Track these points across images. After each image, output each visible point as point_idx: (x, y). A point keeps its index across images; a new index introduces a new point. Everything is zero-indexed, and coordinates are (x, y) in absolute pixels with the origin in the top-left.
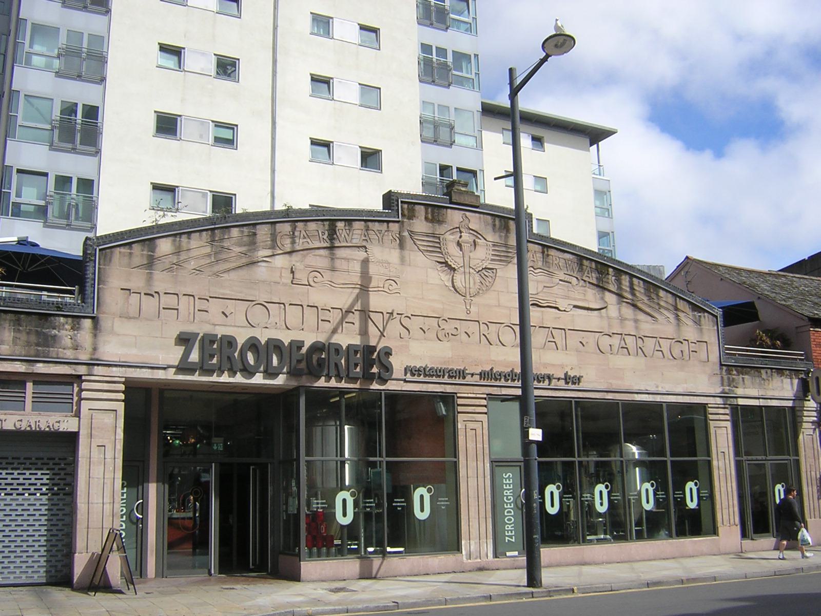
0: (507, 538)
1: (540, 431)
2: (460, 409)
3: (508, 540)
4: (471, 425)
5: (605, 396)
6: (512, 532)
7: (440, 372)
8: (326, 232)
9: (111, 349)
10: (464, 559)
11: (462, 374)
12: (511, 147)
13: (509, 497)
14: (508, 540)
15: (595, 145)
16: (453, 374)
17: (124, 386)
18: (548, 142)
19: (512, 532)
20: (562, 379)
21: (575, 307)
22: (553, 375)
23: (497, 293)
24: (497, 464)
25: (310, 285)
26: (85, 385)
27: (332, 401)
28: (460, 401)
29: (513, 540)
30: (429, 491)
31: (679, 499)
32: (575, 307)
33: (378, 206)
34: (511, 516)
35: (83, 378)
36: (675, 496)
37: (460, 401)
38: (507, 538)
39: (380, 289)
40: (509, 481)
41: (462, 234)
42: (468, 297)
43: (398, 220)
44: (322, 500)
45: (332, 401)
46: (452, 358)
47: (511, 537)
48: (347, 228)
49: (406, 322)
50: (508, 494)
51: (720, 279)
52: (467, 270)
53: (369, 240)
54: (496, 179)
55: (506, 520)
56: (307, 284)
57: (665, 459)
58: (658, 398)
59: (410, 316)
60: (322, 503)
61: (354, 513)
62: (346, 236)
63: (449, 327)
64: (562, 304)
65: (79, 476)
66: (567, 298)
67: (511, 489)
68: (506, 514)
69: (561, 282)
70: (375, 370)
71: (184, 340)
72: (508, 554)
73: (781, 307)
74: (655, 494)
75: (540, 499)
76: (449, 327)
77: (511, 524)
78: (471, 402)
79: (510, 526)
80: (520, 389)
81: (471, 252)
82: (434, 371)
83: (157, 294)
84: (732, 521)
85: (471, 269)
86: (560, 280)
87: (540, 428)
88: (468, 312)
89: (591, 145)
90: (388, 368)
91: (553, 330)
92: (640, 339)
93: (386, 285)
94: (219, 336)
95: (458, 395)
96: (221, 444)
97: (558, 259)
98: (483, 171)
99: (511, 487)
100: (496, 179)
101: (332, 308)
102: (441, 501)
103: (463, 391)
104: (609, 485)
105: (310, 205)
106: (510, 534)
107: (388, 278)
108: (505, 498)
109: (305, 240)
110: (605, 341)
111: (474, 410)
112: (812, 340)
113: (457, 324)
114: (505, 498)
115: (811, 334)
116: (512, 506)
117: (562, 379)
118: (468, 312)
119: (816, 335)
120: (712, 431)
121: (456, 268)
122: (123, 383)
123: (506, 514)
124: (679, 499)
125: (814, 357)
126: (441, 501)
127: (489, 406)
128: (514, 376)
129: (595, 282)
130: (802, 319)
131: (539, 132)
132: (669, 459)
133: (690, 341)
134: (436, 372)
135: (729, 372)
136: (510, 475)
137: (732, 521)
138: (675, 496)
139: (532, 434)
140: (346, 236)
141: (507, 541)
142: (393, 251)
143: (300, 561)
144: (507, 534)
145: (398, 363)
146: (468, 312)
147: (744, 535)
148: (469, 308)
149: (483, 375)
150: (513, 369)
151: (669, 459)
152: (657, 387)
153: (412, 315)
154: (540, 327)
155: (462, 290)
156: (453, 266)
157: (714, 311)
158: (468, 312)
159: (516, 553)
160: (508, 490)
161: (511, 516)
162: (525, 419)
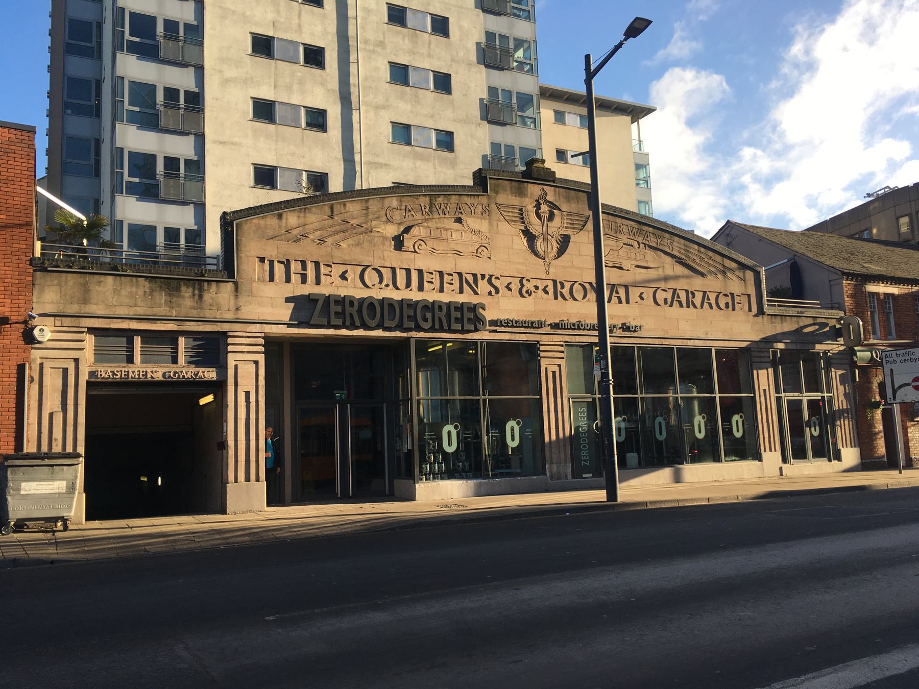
0: (583, 462)
2: (542, 354)
5: (703, 343)
6: (586, 457)
7: (525, 324)
8: (427, 206)
9: (251, 311)
11: (541, 325)
12: (587, 131)
15: (636, 123)
16: (532, 325)
17: (263, 340)
18: (544, 108)
21: (637, 266)
23: (571, 255)
25: (415, 252)
26: (230, 340)
27: (430, 350)
28: (542, 348)
29: (588, 464)
30: (518, 423)
32: (637, 266)
34: (586, 443)
35: (752, 349)
37: (542, 348)
38: (583, 462)
46: (535, 311)
47: (586, 461)
51: (759, 239)
52: (546, 237)
53: (463, 212)
55: (587, 447)
57: (637, 396)
58: (708, 343)
60: (431, 435)
62: (445, 209)
64: (626, 264)
66: (630, 259)
69: (624, 246)
72: (584, 476)
73: (816, 263)
78: (551, 348)
79: (585, 452)
80: (598, 337)
82: (537, 324)
85: (549, 236)
86: (624, 244)
89: (632, 123)
91: (709, 293)
94: (461, 303)
95: (541, 343)
97: (621, 225)
98: (542, 149)
101: (434, 271)
103: (545, 339)
104: (705, 416)
105: (393, 183)
109: (410, 214)
111: (554, 355)
112: (845, 291)
115: (844, 287)
118: (548, 273)
121: (537, 235)
122: (263, 338)
123: (581, 442)
125: (846, 307)
128: (586, 326)
131: (560, 106)
132: (717, 395)
133: (735, 295)
134: (522, 323)
136: (584, 410)
140: (445, 209)
141: (583, 465)
142: (483, 221)
143: (415, 483)
146: (547, 272)
147: (785, 460)
148: (547, 269)
151: (717, 395)
153: (501, 276)
158: (548, 273)
161: (586, 443)
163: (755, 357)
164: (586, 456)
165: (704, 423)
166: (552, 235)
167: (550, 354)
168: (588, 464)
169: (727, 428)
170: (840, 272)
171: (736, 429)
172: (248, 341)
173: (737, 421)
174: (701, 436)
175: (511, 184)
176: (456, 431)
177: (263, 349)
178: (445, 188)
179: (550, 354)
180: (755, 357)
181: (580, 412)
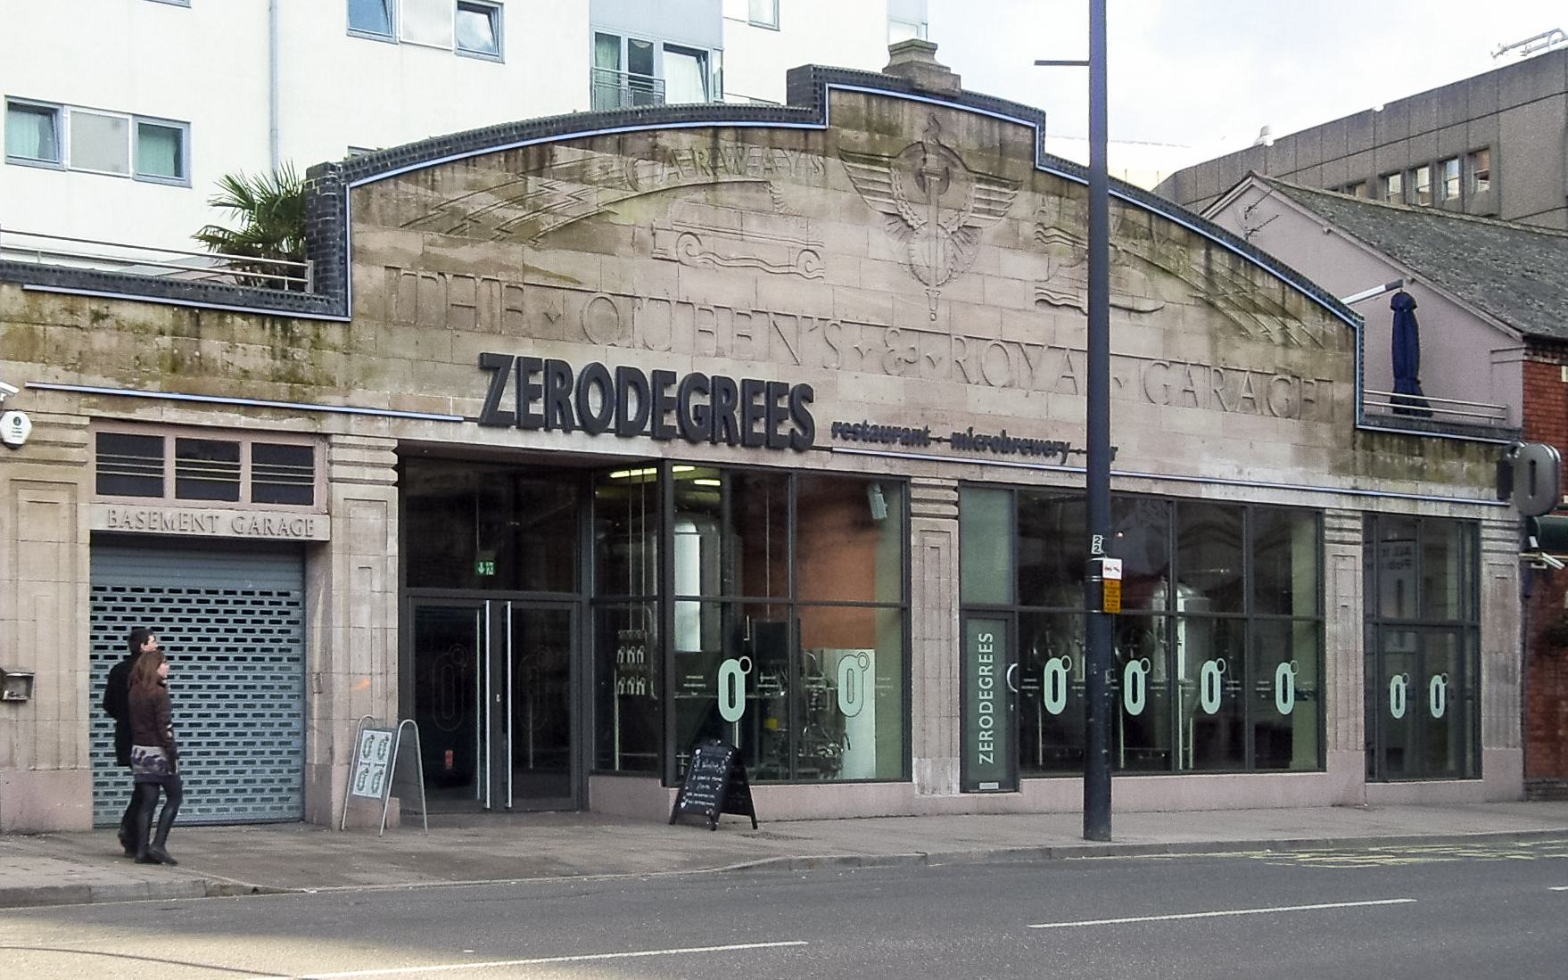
0: (981, 756)
1: (1118, 563)
3: (983, 760)
4: (932, 540)
10: (917, 792)
11: (919, 438)
13: (987, 680)
14: (983, 760)
19: (989, 746)
20: (1084, 452)
22: (1069, 444)
24: (971, 612)
27: (615, 475)
28: (916, 493)
29: (991, 761)
31: (1030, 695)
33: (778, 95)
35: (334, 439)
36: (1023, 687)
37: (916, 493)
38: (981, 756)
39: (792, 269)
40: (988, 648)
41: (927, 156)
42: (933, 284)
43: (823, 127)
44: (1234, 679)
45: (615, 475)
47: (987, 754)
48: (739, 144)
49: (834, 336)
50: (986, 673)
54: (1038, 63)
55: (992, 722)
56: (1029, 350)
59: (839, 323)
61: (747, 701)
63: (901, 346)
65: (393, 622)
67: (990, 664)
68: (981, 711)
70: (783, 430)
71: (492, 365)
72: (982, 786)
74: (1224, 685)
75: (1114, 684)
76: (901, 346)
77: (989, 729)
81: (939, 194)
83: (441, 277)
84: (1352, 743)
87: (1118, 558)
88: (933, 317)
90: (806, 423)
92: (1217, 374)
93: (802, 261)
96: (491, 564)
99: (991, 661)
100: (1038, 63)
102: (691, 681)
103: (919, 474)
106: (986, 749)
107: (805, 247)
108: (981, 679)
110: (1160, 376)
113: (913, 340)
114: (981, 679)
116: (991, 697)
117: (1084, 452)
118: (933, 317)
119: (1532, 369)
120: (1329, 561)
121: (916, 226)
124: (1030, 695)
126: (691, 681)
127: (965, 502)
129: (1145, 255)
130: (1508, 334)
135: (1367, 446)
137: (1352, 743)
138: (1023, 687)
139: (1108, 569)
141: (981, 762)
144: (981, 749)
145: (822, 414)
149: (959, 441)
150: (1004, 432)
152: (1240, 472)
153: (842, 322)
154: (1050, 347)
155: (924, 274)
156: (911, 223)
157: (1350, 318)
158: (933, 317)
159: (996, 786)
160: (986, 665)
162: (1094, 540)
163: (918, 501)
164: (988, 742)
165: (1219, 678)
166: (945, 226)
167: (931, 508)
168: (991, 761)
169: (1030, 691)
170: (1518, 334)
171: (1281, 697)
172: (366, 456)
173: (731, 676)
174: (1211, 708)
175: (981, 123)
176: (744, 673)
177: (393, 476)
178: (742, 111)
179: (931, 508)
180: (918, 501)
181: (982, 643)
